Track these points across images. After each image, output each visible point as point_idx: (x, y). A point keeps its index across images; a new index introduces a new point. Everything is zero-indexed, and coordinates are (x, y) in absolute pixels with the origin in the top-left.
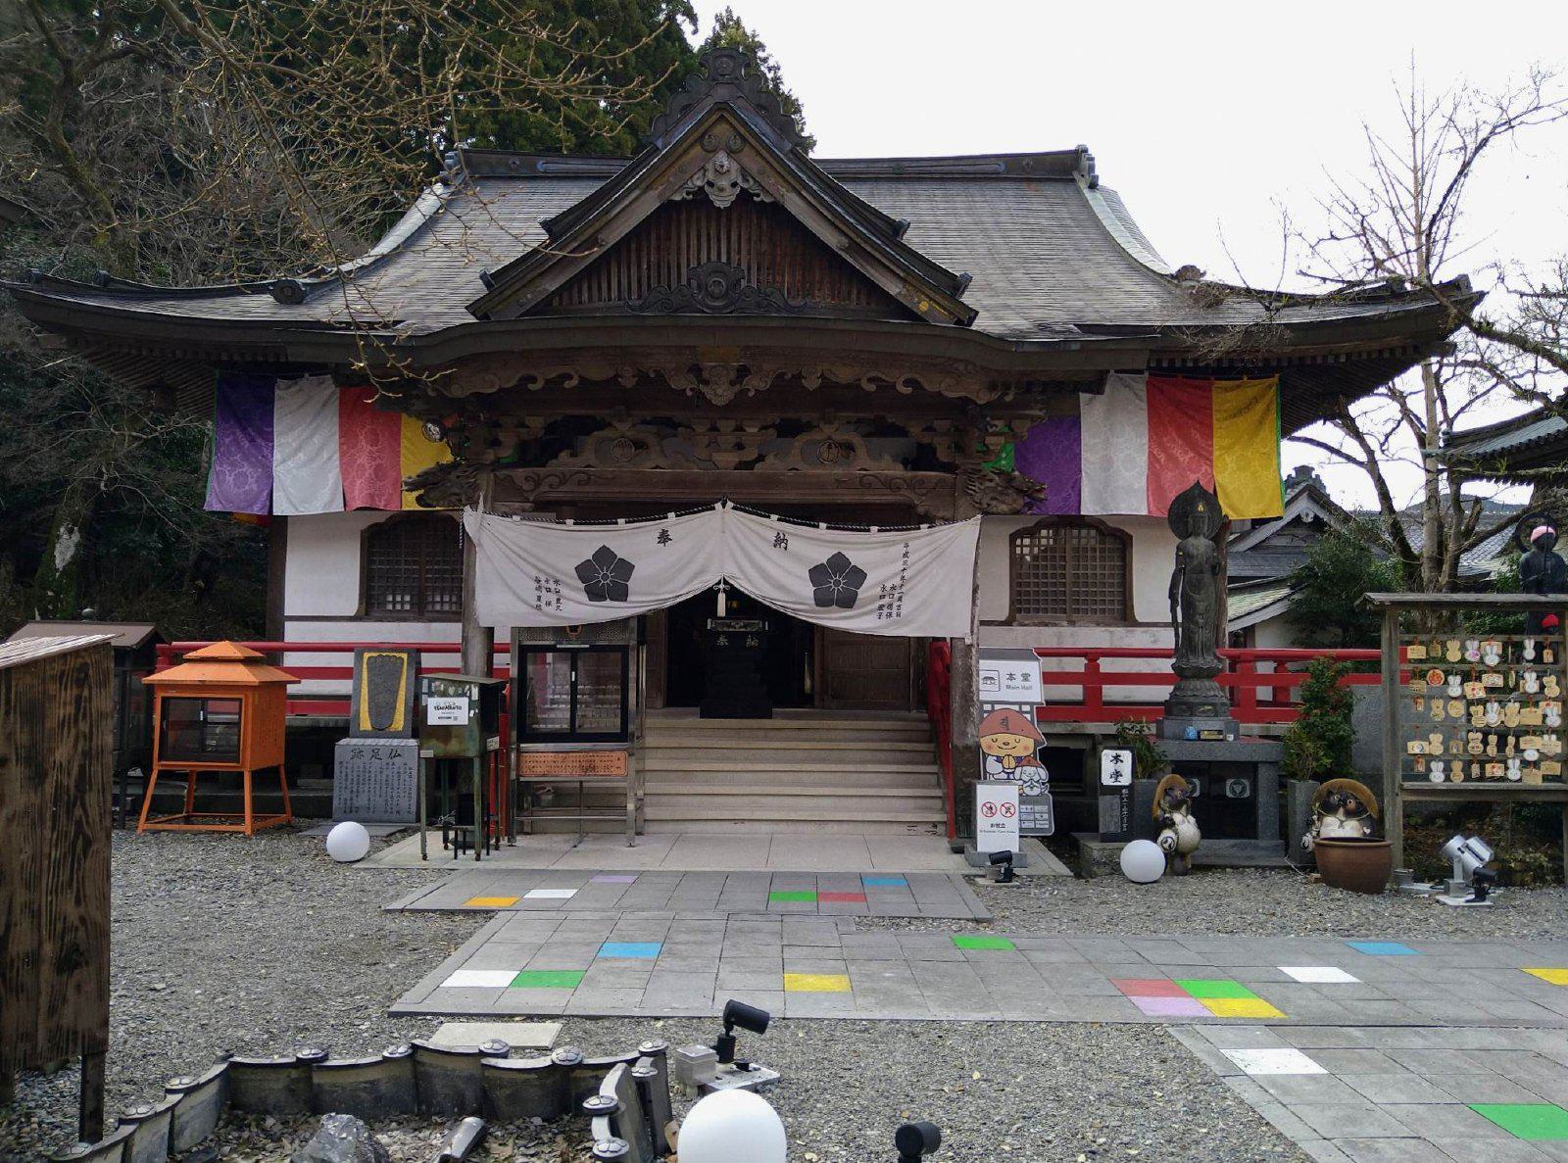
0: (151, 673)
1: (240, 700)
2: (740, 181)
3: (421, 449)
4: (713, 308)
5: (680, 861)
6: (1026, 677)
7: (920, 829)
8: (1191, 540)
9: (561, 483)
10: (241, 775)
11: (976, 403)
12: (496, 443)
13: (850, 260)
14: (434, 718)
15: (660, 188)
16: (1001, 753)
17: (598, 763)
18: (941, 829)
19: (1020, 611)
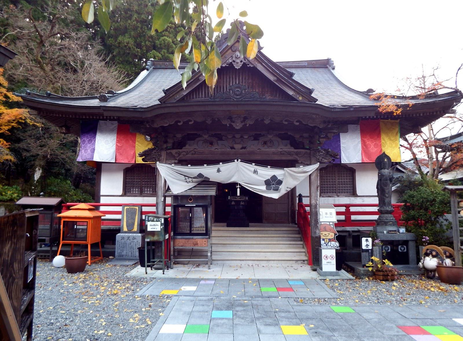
0: (60, 213)
1: (87, 222)
2: (243, 60)
3: (142, 145)
5: (232, 275)
6: (331, 214)
8: (383, 170)
9: (187, 154)
10: (88, 245)
11: (319, 128)
12: (166, 142)
14: (149, 229)
16: (324, 238)
17: (198, 243)
18: (306, 262)
19: (322, 193)
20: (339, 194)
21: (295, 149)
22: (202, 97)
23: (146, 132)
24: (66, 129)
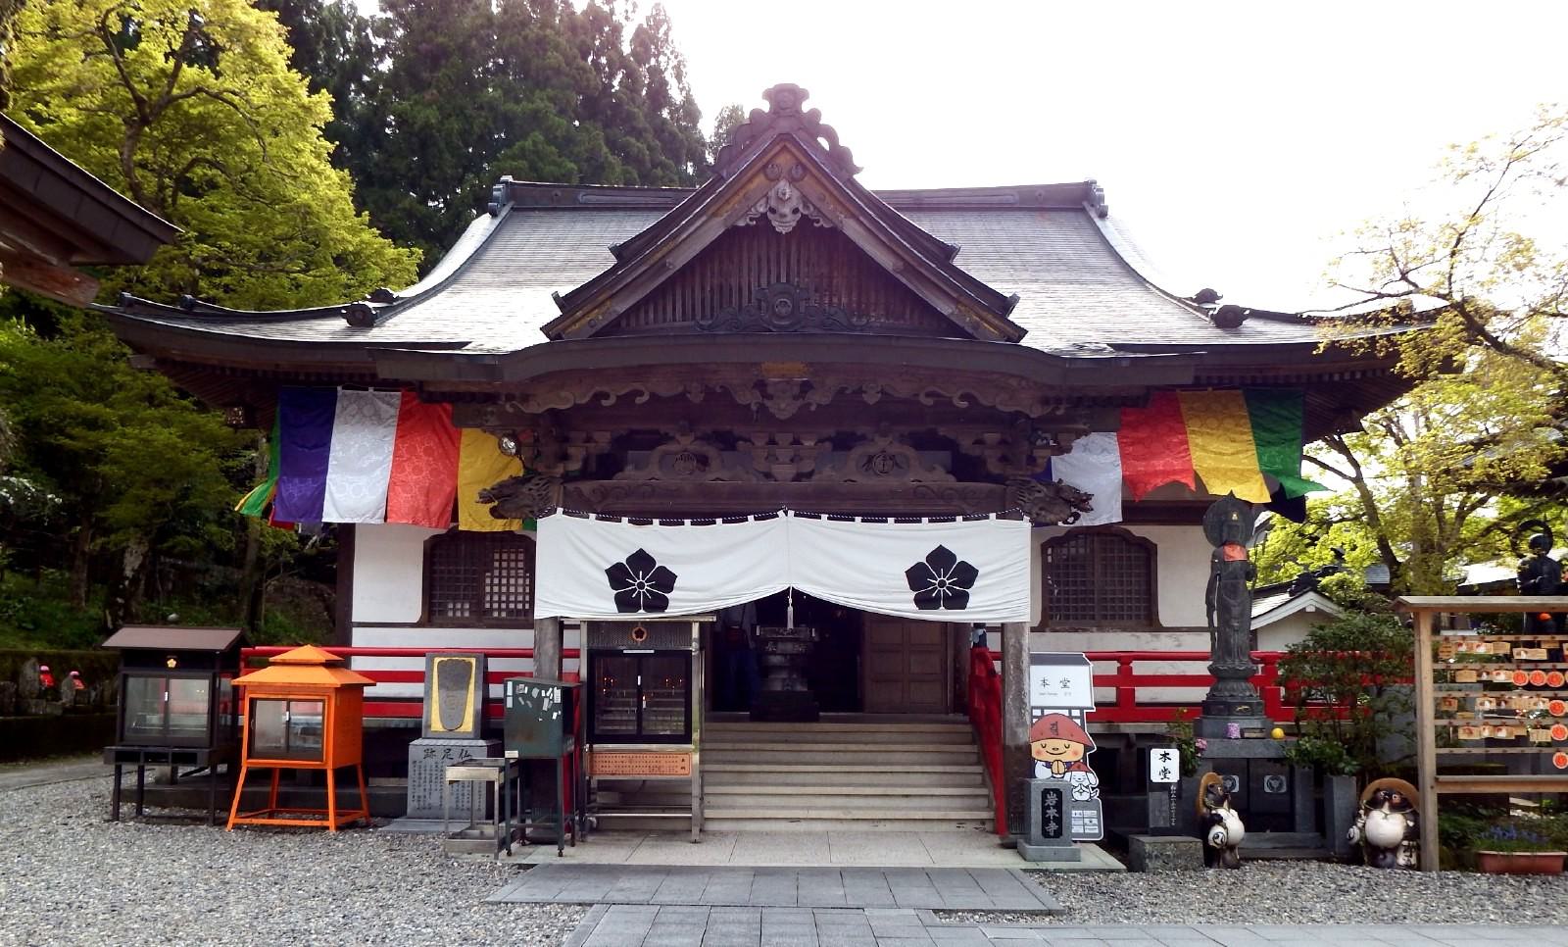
2: (801, 208)
3: (482, 461)
4: (781, 327)
7: (970, 827)
8: (1228, 549)
10: (324, 772)
13: (904, 281)
15: (726, 215)
16: (1051, 758)
20: (1104, 622)
21: (959, 480)
22: (674, 320)
23: (507, 427)
24: (246, 416)
